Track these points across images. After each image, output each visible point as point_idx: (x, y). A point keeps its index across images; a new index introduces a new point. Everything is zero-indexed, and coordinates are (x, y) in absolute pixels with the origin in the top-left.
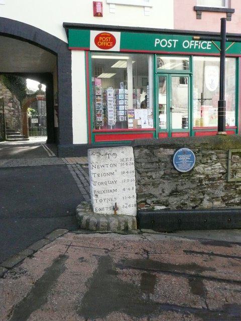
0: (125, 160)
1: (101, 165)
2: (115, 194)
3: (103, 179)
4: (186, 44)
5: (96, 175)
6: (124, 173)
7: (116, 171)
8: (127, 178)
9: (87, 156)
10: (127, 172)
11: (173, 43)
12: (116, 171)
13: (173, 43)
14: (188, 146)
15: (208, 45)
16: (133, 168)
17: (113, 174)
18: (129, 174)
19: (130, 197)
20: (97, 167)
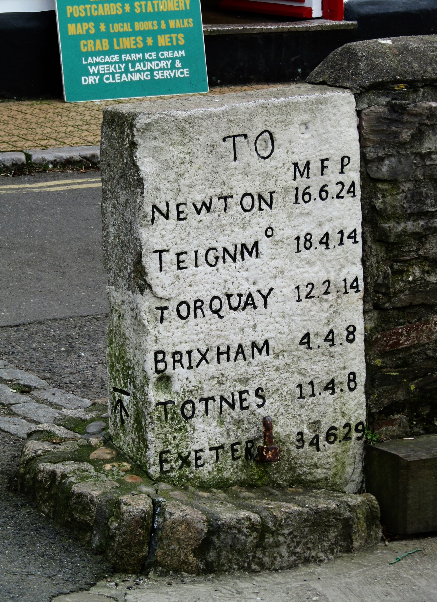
0: (315, 166)
1: (199, 198)
2: (258, 370)
3: (205, 282)
4: (85, 80)
5: (169, 258)
6: (308, 242)
7: (269, 232)
8: (323, 276)
9: (212, 84)
10: (325, 241)
11: (85, 10)
12: (269, 232)
13: (85, 10)
14: (149, 552)
15: (185, 73)
16: (349, 214)
17: (254, 249)
18: (335, 251)
19: (330, 386)
20: (173, 213)
